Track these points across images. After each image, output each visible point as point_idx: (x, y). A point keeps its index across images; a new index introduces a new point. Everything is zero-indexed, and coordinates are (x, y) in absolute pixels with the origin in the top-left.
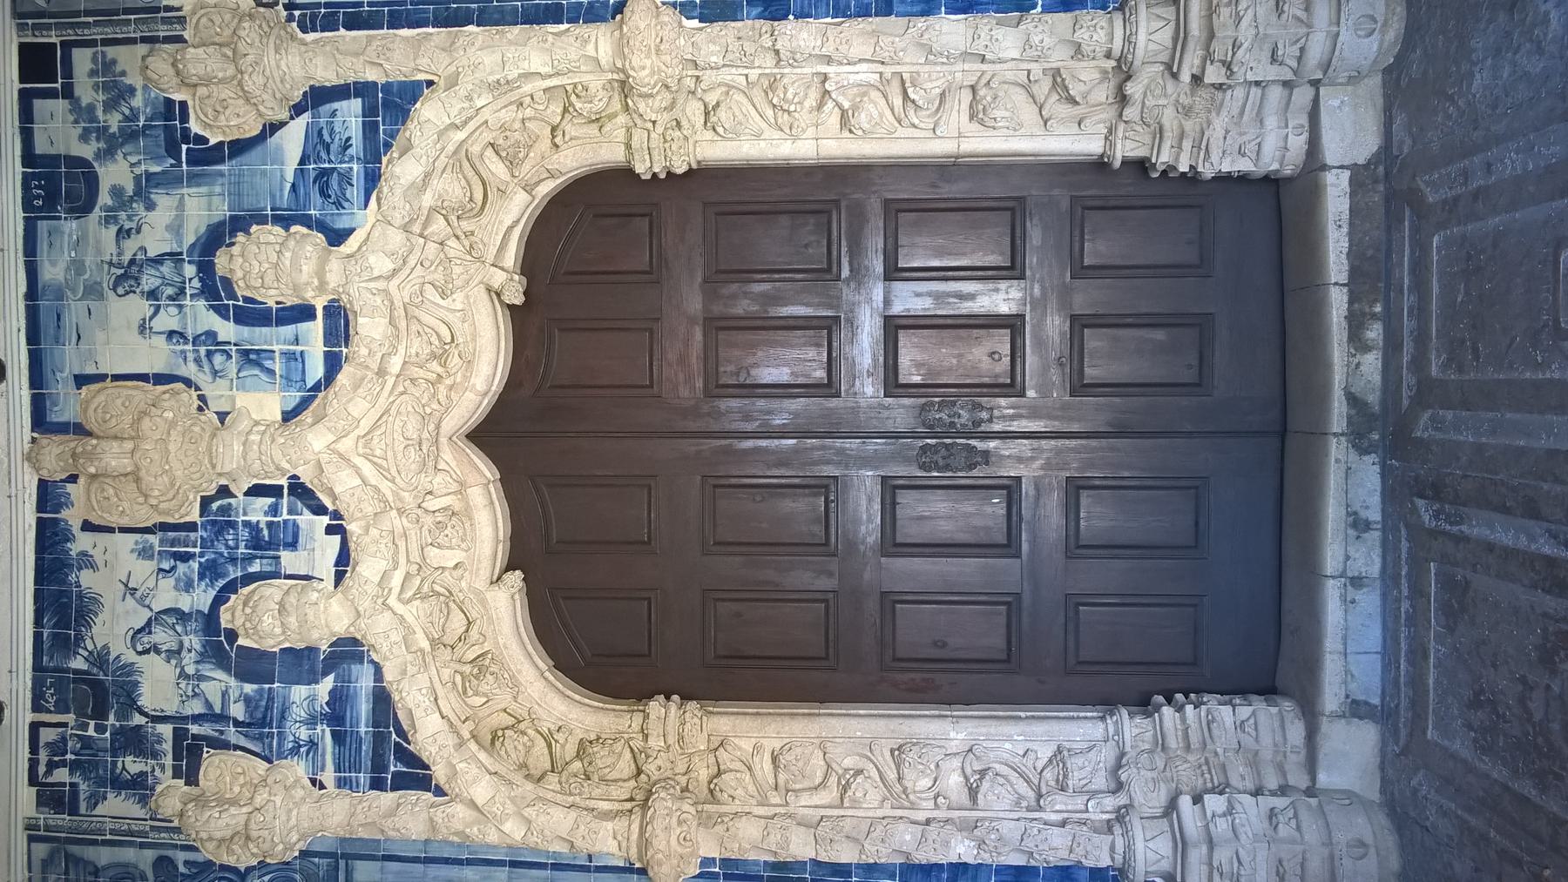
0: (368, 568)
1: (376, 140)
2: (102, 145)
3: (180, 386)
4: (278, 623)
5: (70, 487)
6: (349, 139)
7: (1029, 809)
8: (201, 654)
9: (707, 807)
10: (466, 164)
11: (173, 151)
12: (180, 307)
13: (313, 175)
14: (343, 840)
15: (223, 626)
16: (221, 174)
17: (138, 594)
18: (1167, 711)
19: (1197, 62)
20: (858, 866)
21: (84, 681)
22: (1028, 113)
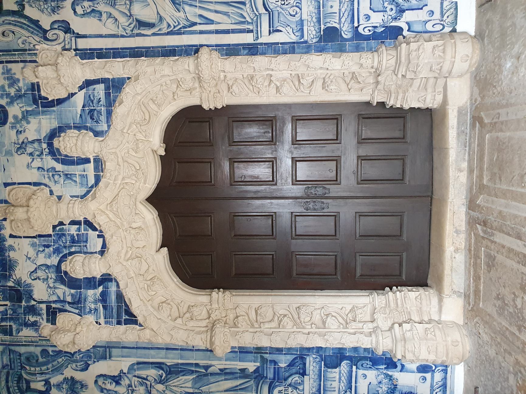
0: (112, 249)
1: (110, 100)
2: (9, 100)
3: (43, 187)
4: (82, 269)
5: (4, 222)
6: (100, 98)
7: (343, 328)
8: (55, 280)
9: (233, 329)
10: (142, 106)
11: (35, 102)
12: (42, 159)
13: (87, 111)
14: (107, 342)
15: (62, 269)
16: (54, 111)
17: (31, 259)
18: (390, 294)
19: (404, 70)
20: (285, 348)
21: (14, 290)
22: (344, 86)
